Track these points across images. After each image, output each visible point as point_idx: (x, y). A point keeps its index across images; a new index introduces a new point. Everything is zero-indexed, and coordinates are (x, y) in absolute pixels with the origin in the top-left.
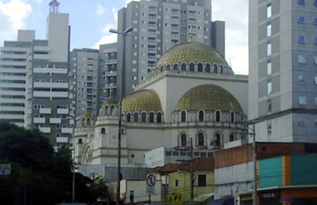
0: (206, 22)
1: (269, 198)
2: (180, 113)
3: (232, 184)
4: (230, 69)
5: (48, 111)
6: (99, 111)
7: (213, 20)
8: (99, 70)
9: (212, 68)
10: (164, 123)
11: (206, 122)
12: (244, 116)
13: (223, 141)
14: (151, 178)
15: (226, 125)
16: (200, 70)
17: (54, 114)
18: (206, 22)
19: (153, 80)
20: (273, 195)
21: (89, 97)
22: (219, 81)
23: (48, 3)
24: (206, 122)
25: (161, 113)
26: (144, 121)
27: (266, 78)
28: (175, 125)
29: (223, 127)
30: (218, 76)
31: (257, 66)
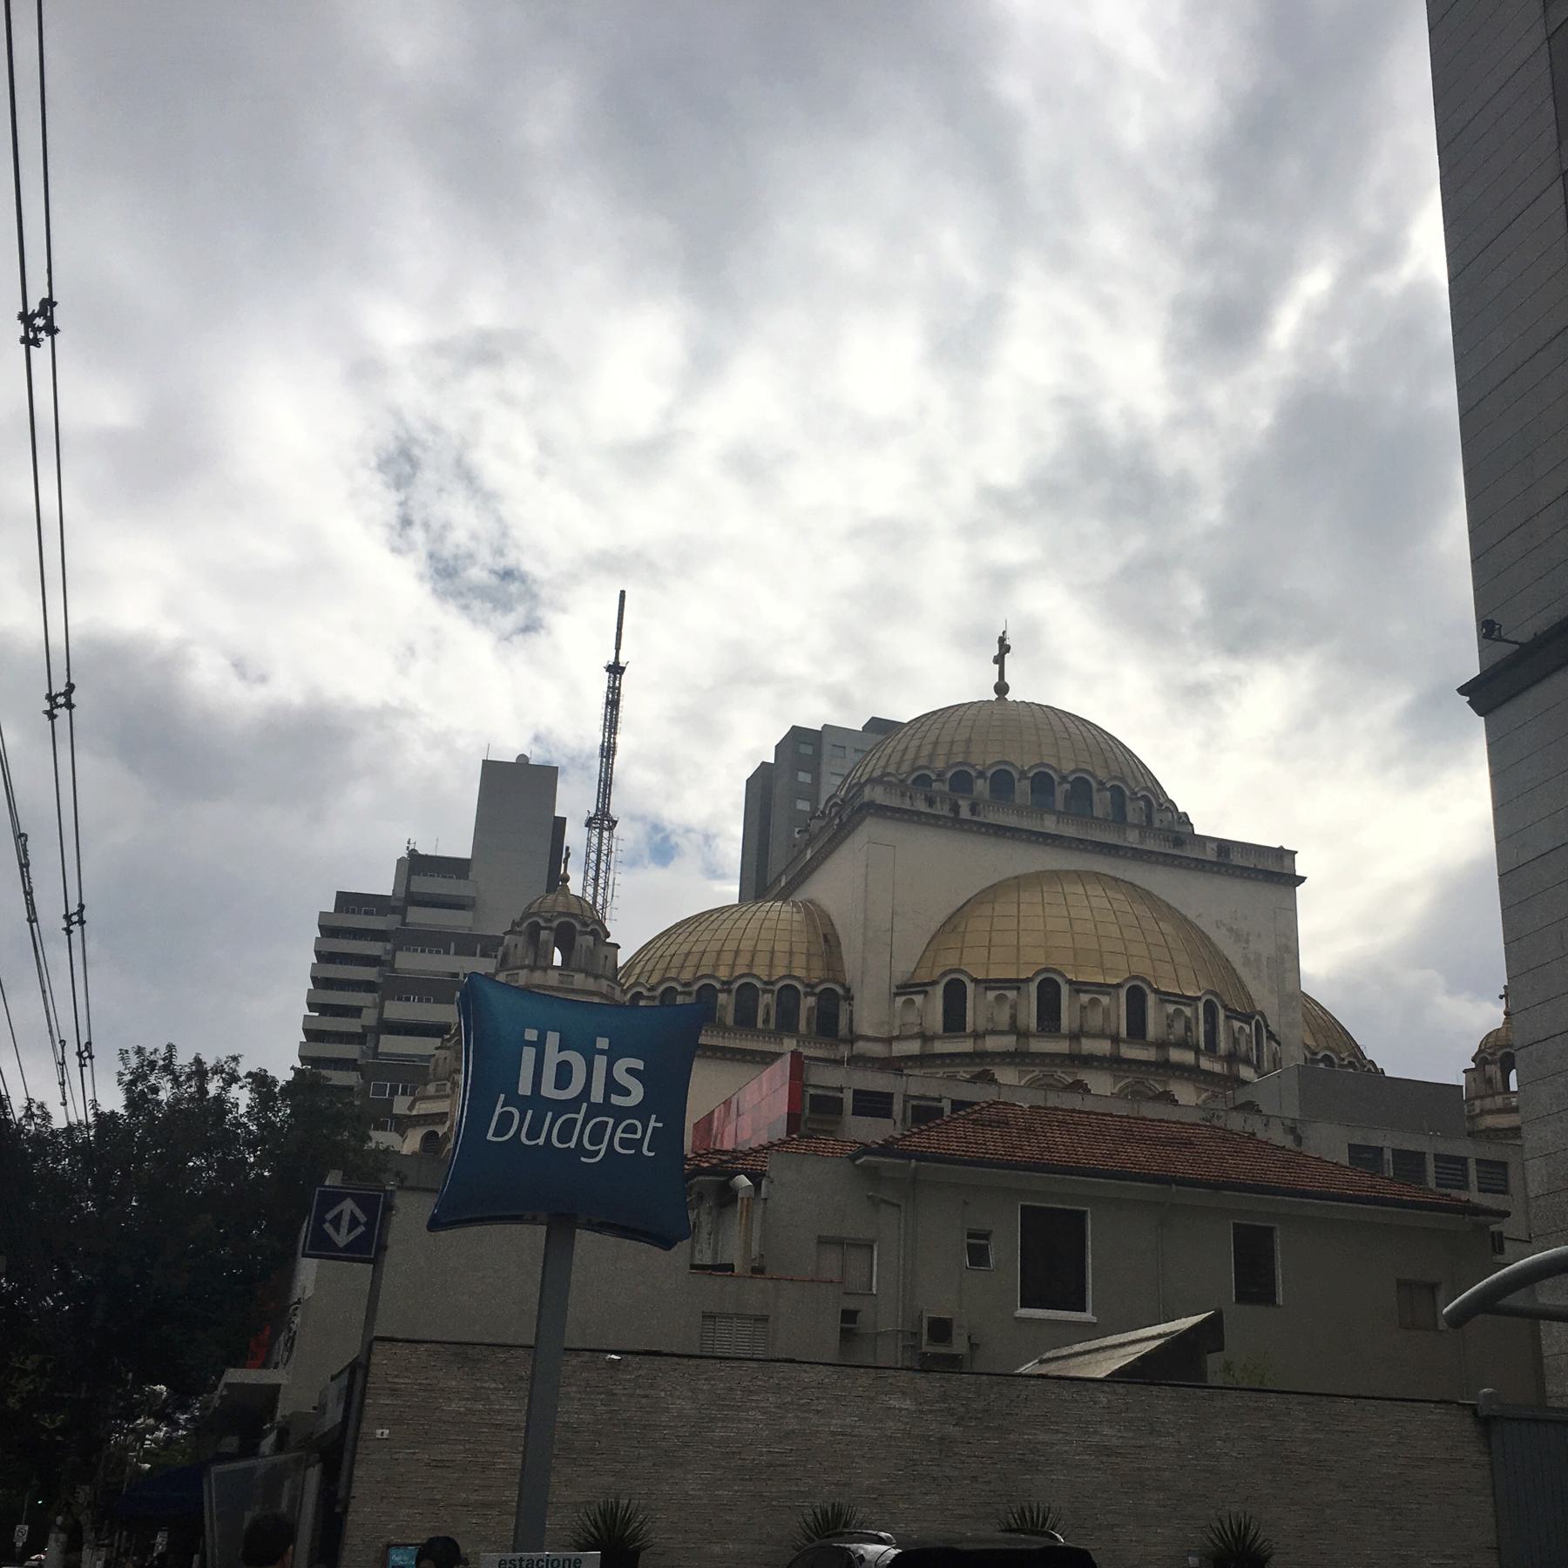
10: (853, 1038)
11: (1075, 1037)
23: (585, 817)
25: (840, 991)
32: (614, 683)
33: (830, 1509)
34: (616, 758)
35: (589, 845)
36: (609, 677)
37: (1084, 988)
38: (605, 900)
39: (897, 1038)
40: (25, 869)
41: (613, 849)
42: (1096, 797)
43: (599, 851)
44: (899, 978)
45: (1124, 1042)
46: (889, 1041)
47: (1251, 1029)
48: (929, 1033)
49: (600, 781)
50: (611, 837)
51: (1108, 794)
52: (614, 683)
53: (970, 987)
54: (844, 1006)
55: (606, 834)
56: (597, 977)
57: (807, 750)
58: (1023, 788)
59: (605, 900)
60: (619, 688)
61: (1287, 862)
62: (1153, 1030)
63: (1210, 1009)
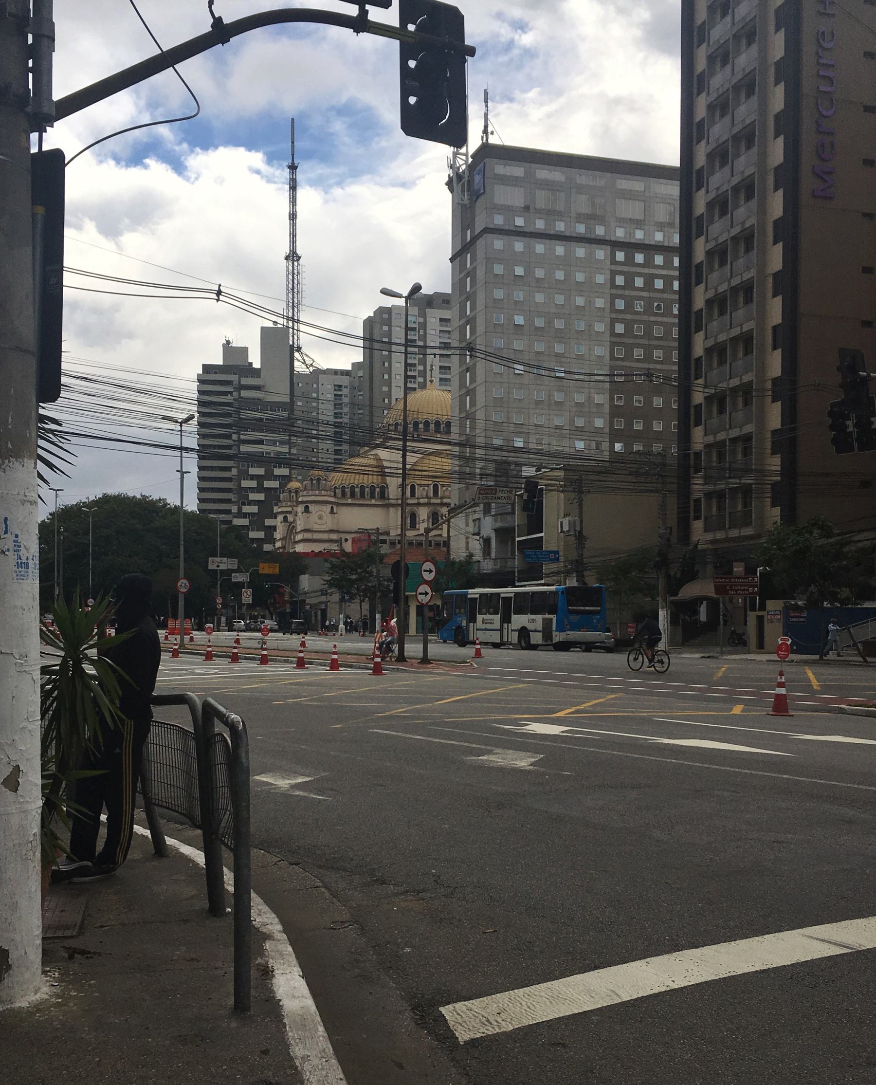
5: (261, 471)
10: (389, 499)
11: (442, 498)
13: (404, 588)
17: (269, 476)
22: (315, 544)
23: (284, 255)
24: (442, 498)
25: (385, 486)
26: (362, 496)
32: (293, 175)
34: (297, 220)
35: (287, 271)
36: (290, 172)
38: (298, 301)
41: (300, 272)
43: (293, 274)
49: (290, 234)
50: (299, 265)
52: (293, 175)
53: (416, 486)
54: (386, 489)
55: (296, 263)
56: (327, 491)
57: (386, 316)
58: (432, 426)
59: (298, 301)
60: (296, 179)
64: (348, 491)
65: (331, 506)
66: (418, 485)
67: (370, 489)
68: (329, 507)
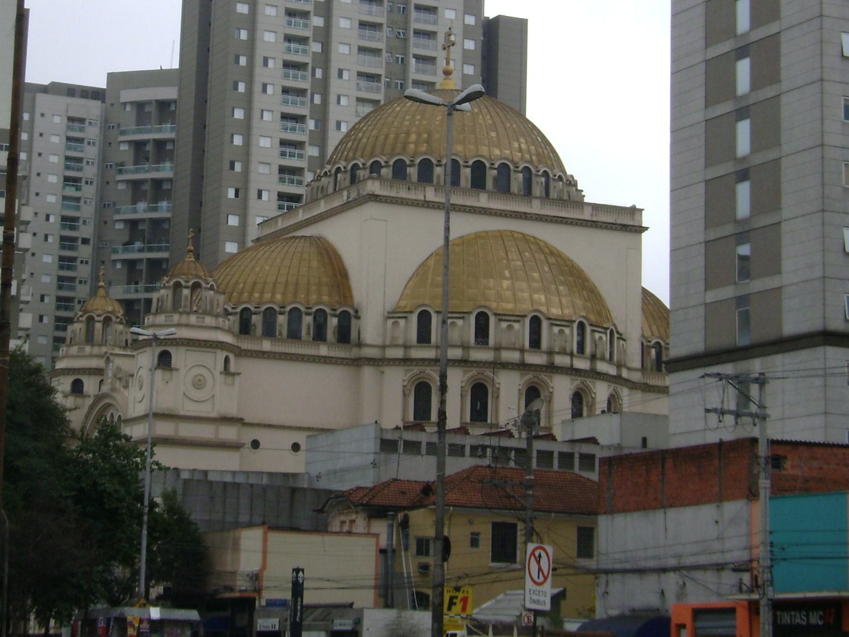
0: (470, 20)
1: (799, 626)
2: (414, 319)
3: (664, 570)
4: (571, 183)
6: (627, 380)
7: (490, 12)
8: (104, 158)
9: (517, 180)
10: (360, 345)
11: (550, 353)
12: (616, 335)
14: (540, 556)
15: (513, 356)
16: (478, 183)
18: (470, 20)
19: (323, 207)
20: (815, 619)
21: (67, 242)
24: (498, 349)
26: (294, 335)
27: (729, 229)
28: (399, 353)
29: (552, 368)
30: (536, 207)
31: (701, 189)
33: (78, 331)
37: (504, 318)
39: (389, 346)
40: (298, 620)
42: (513, 176)
44: (389, 307)
45: (528, 351)
46: (383, 347)
47: (607, 336)
48: (408, 344)
51: (521, 175)
61: (637, 217)
62: (545, 344)
63: (581, 326)
64: (256, 320)
65: (225, 354)
66: (496, 314)
67: (315, 318)
68: (221, 355)
